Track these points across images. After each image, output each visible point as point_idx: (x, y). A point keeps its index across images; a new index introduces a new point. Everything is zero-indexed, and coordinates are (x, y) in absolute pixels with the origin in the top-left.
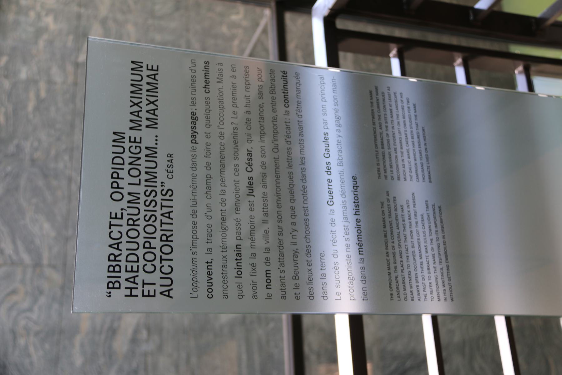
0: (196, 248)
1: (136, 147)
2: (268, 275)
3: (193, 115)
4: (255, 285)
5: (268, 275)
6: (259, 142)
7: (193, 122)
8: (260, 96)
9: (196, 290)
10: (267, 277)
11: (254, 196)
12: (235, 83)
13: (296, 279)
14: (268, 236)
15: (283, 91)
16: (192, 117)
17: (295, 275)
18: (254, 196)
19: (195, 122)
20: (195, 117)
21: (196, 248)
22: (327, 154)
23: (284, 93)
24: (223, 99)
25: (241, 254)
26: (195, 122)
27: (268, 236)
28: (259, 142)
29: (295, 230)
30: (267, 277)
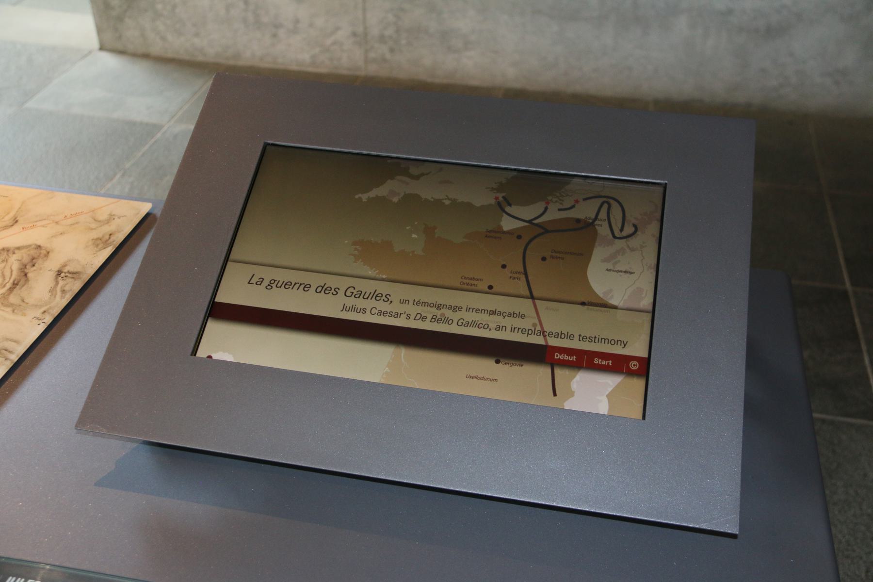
0: (511, 331)
1: (463, 323)
2: (483, 311)
3: (459, 308)
4: (566, 337)
5: (483, 311)
6: (512, 325)
7: (451, 307)
8: (393, 314)
9: (451, 321)
10: (618, 341)
11: (341, 311)
12: (401, 316)
13: (432, 318)
14: (353, 310)
15: (597, 337)
16: (457, 307)
17: (436, 319)
18: (341, 311)
19: (451, 309)
20: (457, 309)
21: (511, 331)
22: (463, 323)
23: (595, 338)
24: (595, 342)
25: (499, 330)
26: (451, 309)
27: (353, 310)
28: (512, 325)
29: (625, 346)
30: (618, 341)
